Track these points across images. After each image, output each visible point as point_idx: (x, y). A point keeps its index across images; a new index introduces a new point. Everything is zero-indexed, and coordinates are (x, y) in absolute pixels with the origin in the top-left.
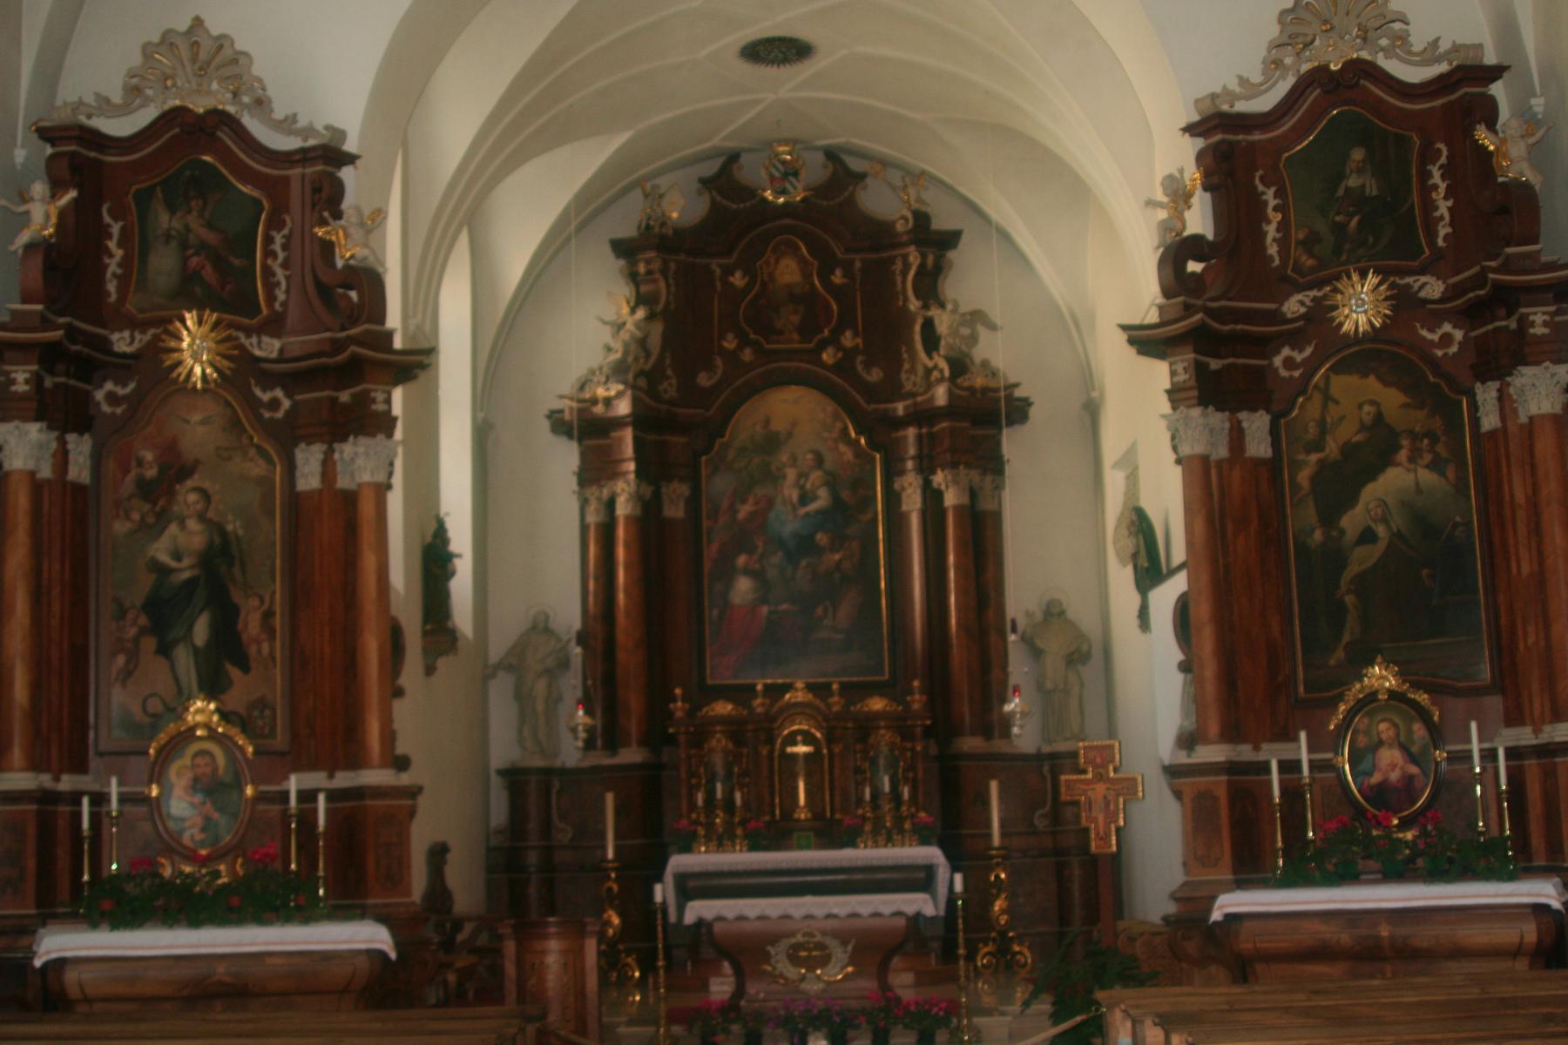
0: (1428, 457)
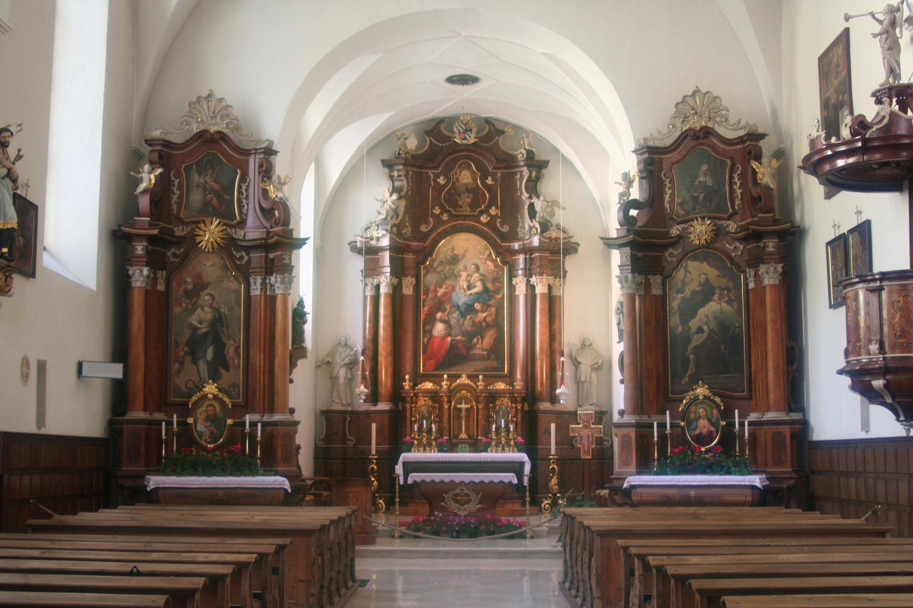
0: (726, 298)
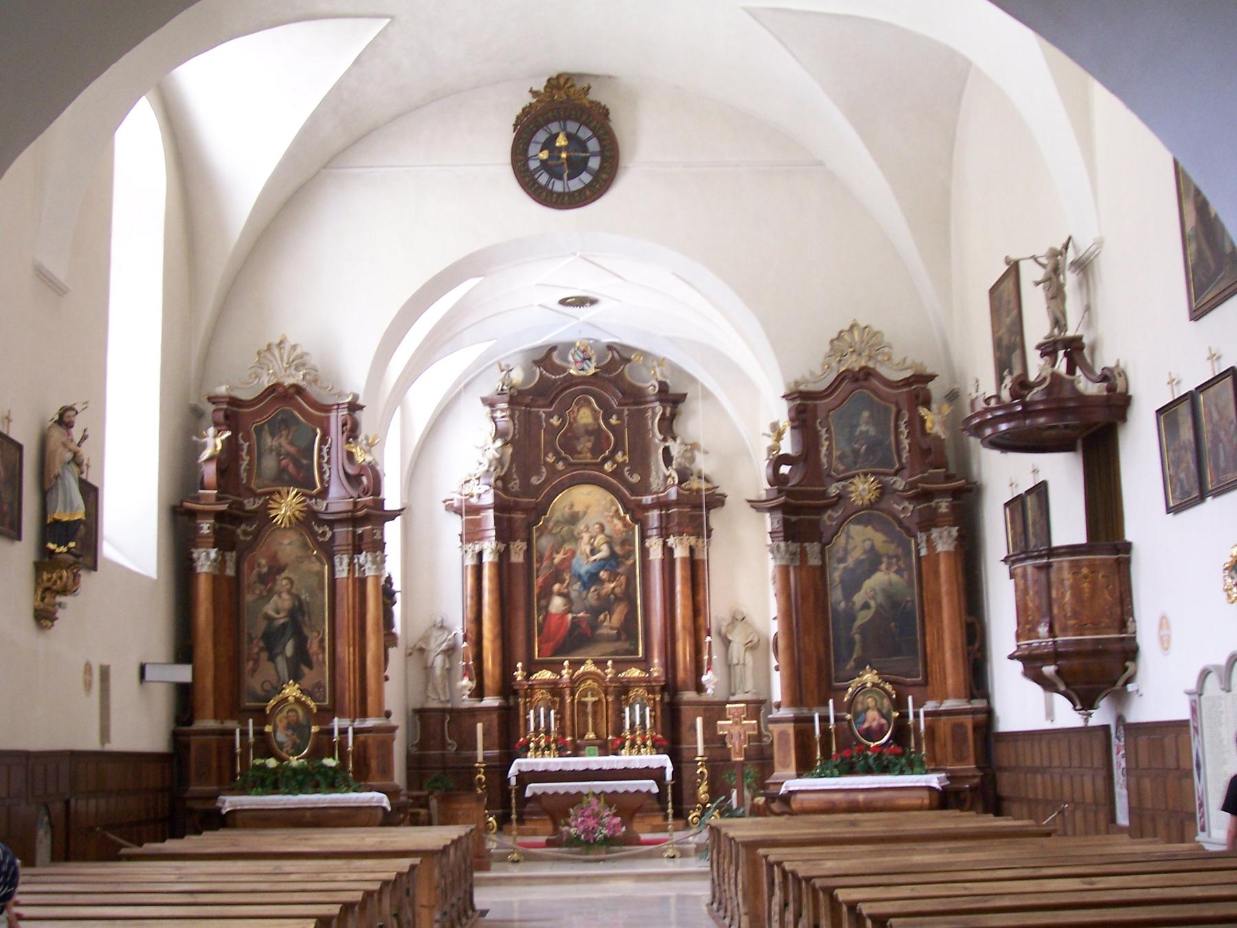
0: (895, 568)
